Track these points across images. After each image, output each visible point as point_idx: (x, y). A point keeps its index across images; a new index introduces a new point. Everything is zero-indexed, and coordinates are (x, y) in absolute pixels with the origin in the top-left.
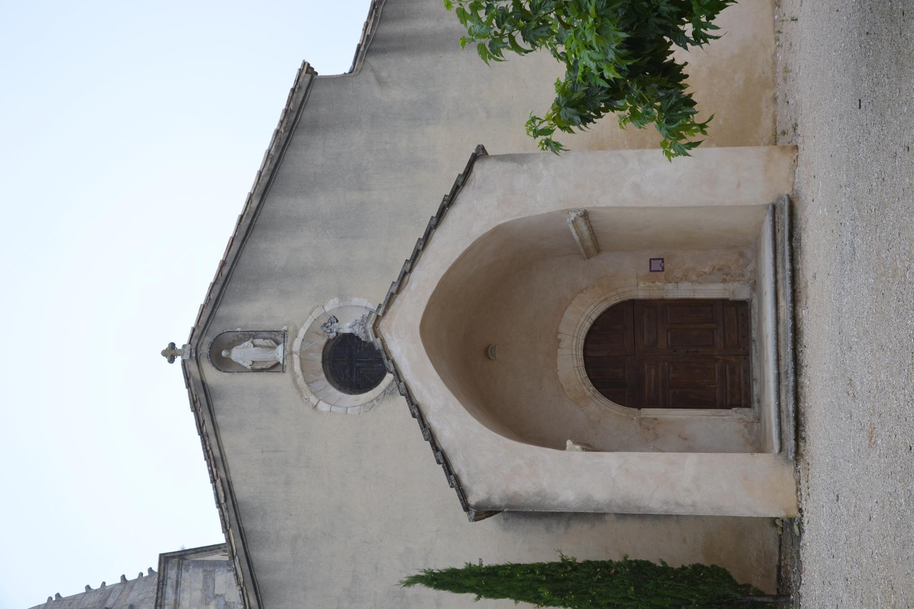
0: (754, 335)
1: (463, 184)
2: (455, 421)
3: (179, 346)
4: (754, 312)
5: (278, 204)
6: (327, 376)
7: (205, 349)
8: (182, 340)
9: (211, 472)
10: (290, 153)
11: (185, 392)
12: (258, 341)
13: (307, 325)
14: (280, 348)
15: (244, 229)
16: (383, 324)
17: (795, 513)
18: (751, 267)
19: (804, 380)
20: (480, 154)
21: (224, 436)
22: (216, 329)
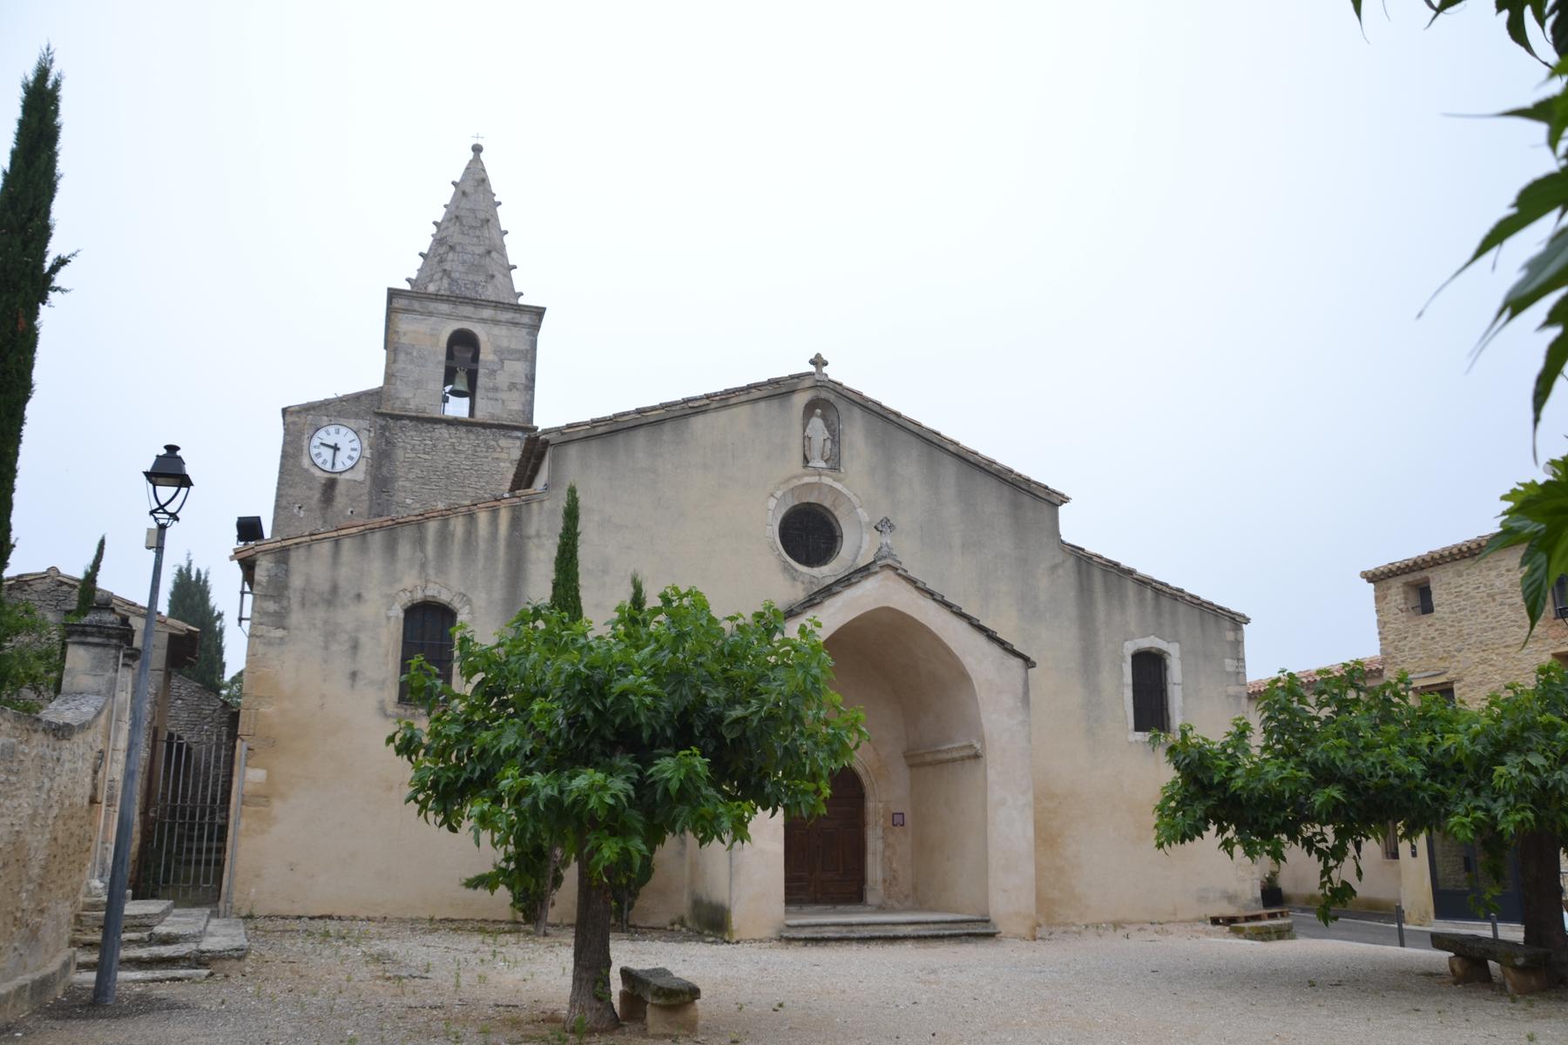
0: (840, 907)
1: (1006, 649)
3: (825, 370)
4: (859, 907)
5: (950, 468)
7: (824, 394)
8: (833, 372)
9: (716, 395)
10: (994, 482)
11: (786, 374)
12: (829, 444)
13: (845, 491)
14: (823, 464)
15: (929, 436)
16: (890, 573)
17: (736, 937)
18: (896, 905)
19: (855, 946)
20: (1028, 662)
21: (746, 409)
22: (841, 406)
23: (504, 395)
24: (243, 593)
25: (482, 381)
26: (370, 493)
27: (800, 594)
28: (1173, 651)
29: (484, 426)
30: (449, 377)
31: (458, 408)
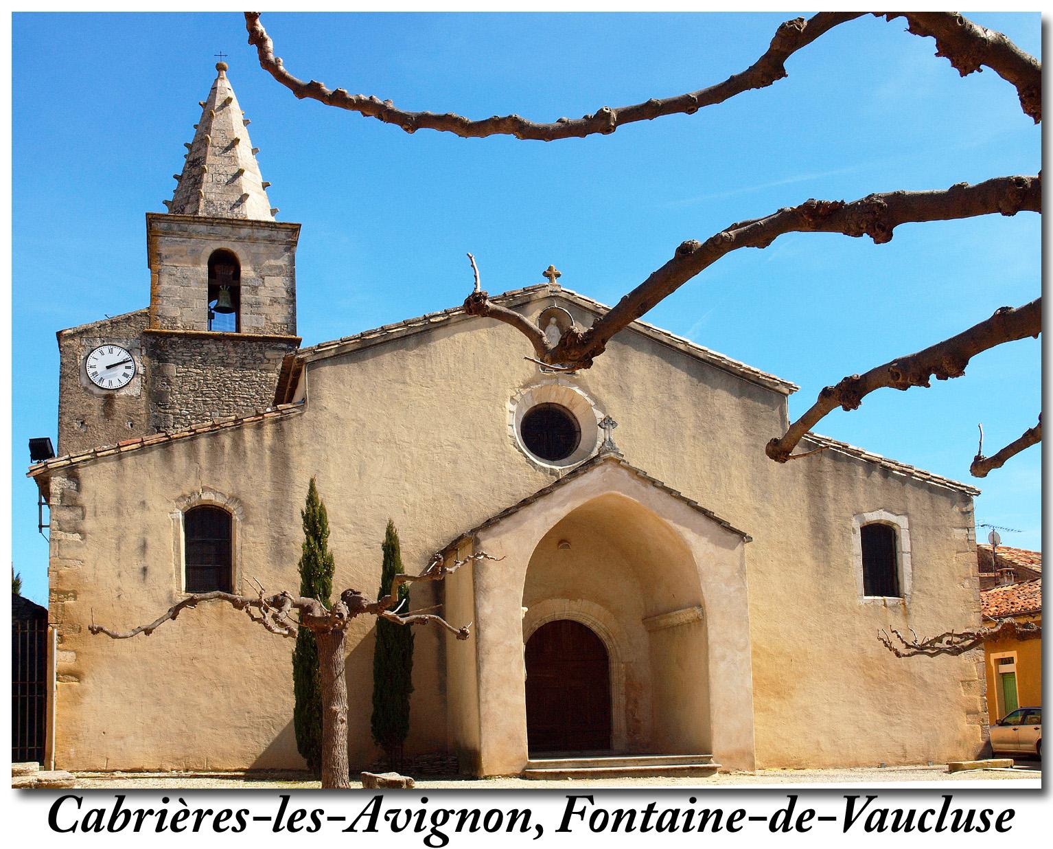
2: (540, 522)
6: (535, 407)
23: (266, 309)
24: (40, 504)
25: (245, 296)
26: (147, 408)
27: (542, 481)
28: (901, 523)
29: (251, 339)
30: (213, 293)
31: (224, 324)
